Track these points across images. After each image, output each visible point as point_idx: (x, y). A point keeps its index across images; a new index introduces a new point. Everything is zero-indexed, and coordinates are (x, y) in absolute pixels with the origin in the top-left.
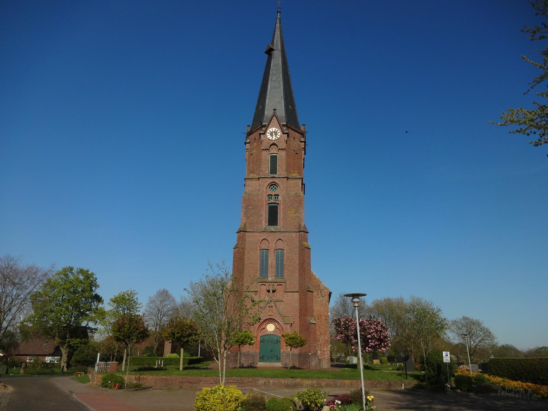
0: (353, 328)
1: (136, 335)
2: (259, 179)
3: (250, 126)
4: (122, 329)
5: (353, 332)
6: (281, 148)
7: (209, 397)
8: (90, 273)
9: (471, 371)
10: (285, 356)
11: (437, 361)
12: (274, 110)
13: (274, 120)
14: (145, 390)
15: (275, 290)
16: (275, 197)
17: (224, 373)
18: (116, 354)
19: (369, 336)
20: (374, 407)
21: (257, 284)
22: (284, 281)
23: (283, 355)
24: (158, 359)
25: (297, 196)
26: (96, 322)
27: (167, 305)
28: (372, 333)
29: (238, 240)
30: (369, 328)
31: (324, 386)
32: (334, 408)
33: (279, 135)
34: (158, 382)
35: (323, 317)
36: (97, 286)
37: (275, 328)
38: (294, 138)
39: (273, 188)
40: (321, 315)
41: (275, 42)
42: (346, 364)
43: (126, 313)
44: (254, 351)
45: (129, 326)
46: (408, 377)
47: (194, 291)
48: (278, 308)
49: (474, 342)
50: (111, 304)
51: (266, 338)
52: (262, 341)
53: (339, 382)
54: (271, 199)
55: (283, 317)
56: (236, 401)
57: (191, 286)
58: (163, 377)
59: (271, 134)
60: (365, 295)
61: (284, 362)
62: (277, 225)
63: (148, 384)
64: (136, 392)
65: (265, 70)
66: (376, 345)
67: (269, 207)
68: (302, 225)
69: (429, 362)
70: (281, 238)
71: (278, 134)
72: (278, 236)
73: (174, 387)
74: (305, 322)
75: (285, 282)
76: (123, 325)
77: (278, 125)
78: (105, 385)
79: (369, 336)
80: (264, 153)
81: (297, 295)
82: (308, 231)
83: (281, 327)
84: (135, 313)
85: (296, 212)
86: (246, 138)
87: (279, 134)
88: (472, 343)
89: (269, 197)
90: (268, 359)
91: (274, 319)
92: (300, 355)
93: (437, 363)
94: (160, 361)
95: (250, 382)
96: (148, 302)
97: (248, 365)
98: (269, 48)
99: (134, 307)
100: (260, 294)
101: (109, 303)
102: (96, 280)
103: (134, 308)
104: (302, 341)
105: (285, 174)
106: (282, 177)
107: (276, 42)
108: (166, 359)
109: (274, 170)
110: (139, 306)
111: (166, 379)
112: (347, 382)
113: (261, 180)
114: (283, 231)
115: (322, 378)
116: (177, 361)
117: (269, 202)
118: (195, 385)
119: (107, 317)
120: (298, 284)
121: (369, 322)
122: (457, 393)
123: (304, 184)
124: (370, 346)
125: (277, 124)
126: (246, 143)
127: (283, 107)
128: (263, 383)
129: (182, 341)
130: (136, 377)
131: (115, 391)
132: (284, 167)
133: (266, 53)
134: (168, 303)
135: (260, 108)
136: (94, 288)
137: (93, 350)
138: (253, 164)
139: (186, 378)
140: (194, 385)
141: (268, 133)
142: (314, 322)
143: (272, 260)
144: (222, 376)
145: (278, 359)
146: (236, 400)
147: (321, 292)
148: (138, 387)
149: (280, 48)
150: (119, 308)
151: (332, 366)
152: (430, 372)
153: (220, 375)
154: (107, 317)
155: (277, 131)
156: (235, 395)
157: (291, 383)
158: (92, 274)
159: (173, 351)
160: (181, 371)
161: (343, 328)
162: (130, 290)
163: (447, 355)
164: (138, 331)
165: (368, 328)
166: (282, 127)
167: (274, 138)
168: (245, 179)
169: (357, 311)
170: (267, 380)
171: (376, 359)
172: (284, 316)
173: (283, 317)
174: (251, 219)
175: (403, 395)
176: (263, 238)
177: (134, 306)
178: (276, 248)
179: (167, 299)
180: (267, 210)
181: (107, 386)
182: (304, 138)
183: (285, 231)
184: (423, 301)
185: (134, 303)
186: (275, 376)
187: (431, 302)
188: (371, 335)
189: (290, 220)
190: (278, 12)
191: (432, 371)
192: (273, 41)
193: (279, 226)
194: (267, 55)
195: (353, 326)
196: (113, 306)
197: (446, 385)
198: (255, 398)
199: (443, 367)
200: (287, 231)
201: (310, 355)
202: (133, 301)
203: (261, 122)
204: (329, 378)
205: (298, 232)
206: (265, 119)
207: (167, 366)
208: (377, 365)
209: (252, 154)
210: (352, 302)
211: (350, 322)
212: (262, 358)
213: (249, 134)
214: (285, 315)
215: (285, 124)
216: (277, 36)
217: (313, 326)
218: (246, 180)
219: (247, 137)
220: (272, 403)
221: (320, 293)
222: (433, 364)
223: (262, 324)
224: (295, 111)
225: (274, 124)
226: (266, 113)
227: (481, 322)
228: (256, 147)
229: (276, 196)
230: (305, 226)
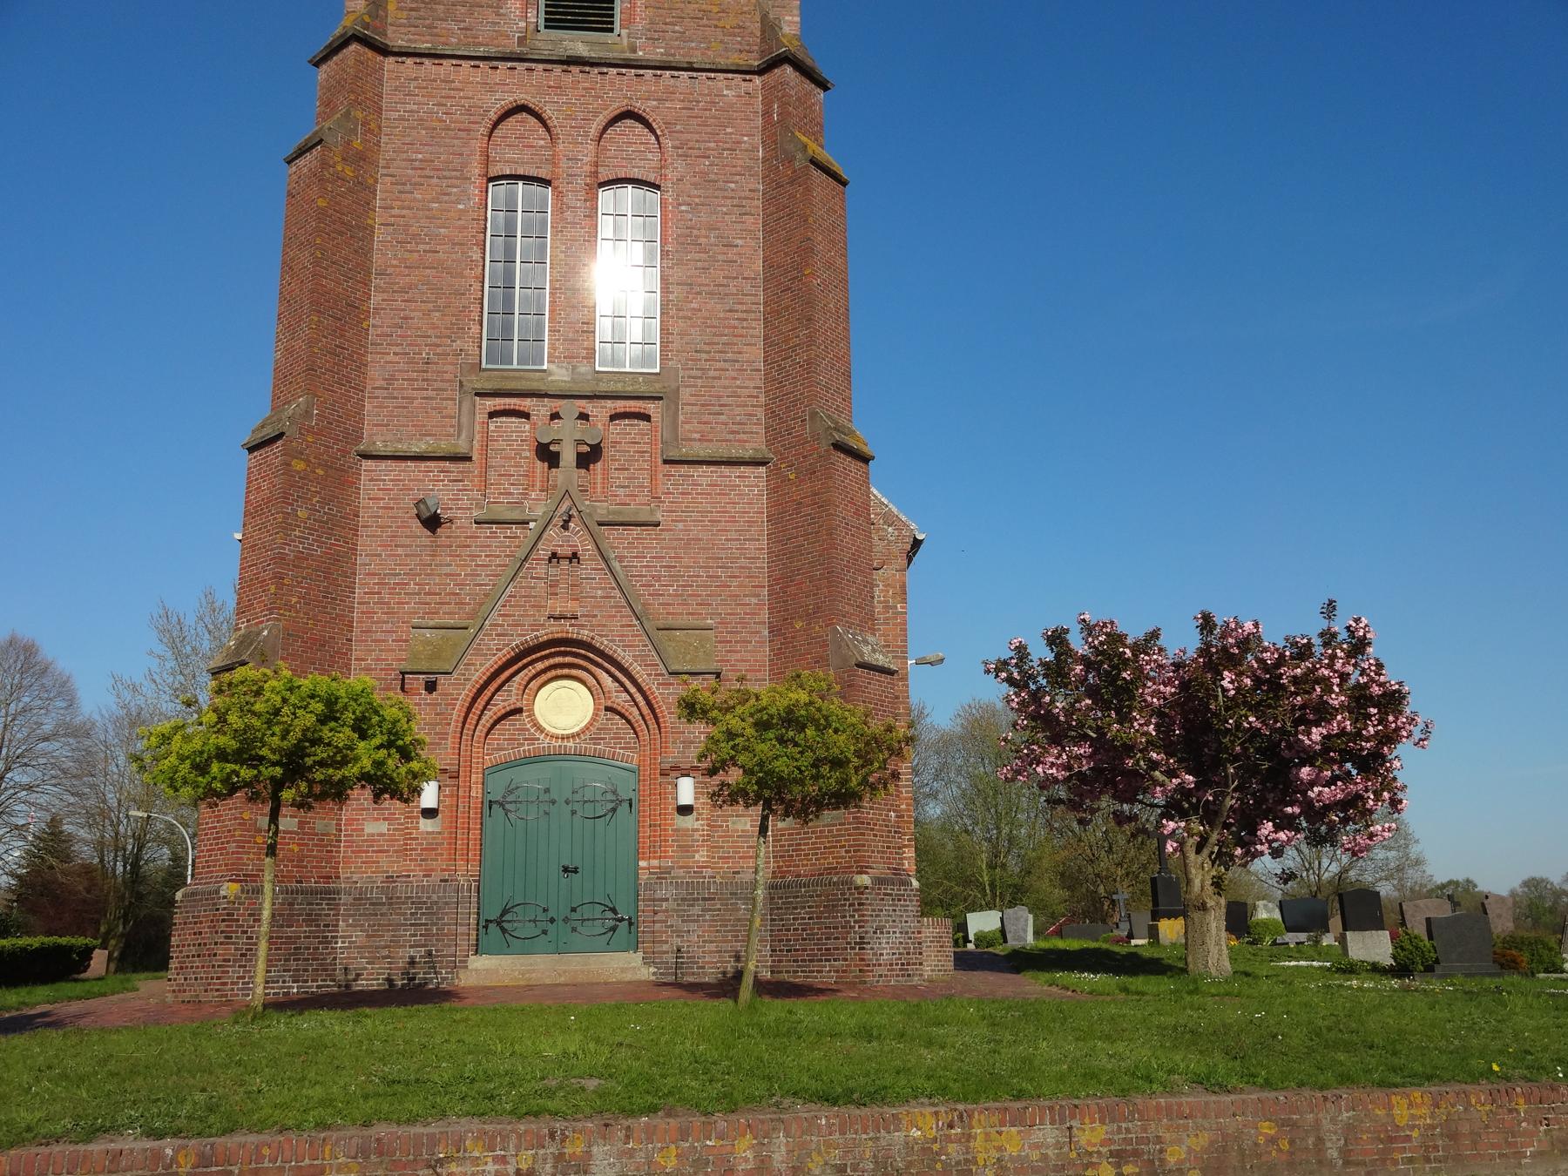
10: (672, 905)
21: (466, 406)
23: (659, 894)
37: (596, 709)
44: (436, 877)
48: (616, 565)
51: (532, 779)
52: (502, 805)
55: (658, 633)
61: (665, 947)
70: (639, 106)
72: (619, 90)
83: (639, 698)
90: (545, 932)
91: (589, 646)
97: (390, 981)
100: (484, 476)
120: (760, 413)
165: (1295, 680)
170: (552, 1149)
172: (661, 624)
173: (658, 633)
176: (508, 100)
193: (624, 32)
201: (861, 890)
205: (760, 72)
212: (499, 923)
214: (671, 622)
223: (499, 681)
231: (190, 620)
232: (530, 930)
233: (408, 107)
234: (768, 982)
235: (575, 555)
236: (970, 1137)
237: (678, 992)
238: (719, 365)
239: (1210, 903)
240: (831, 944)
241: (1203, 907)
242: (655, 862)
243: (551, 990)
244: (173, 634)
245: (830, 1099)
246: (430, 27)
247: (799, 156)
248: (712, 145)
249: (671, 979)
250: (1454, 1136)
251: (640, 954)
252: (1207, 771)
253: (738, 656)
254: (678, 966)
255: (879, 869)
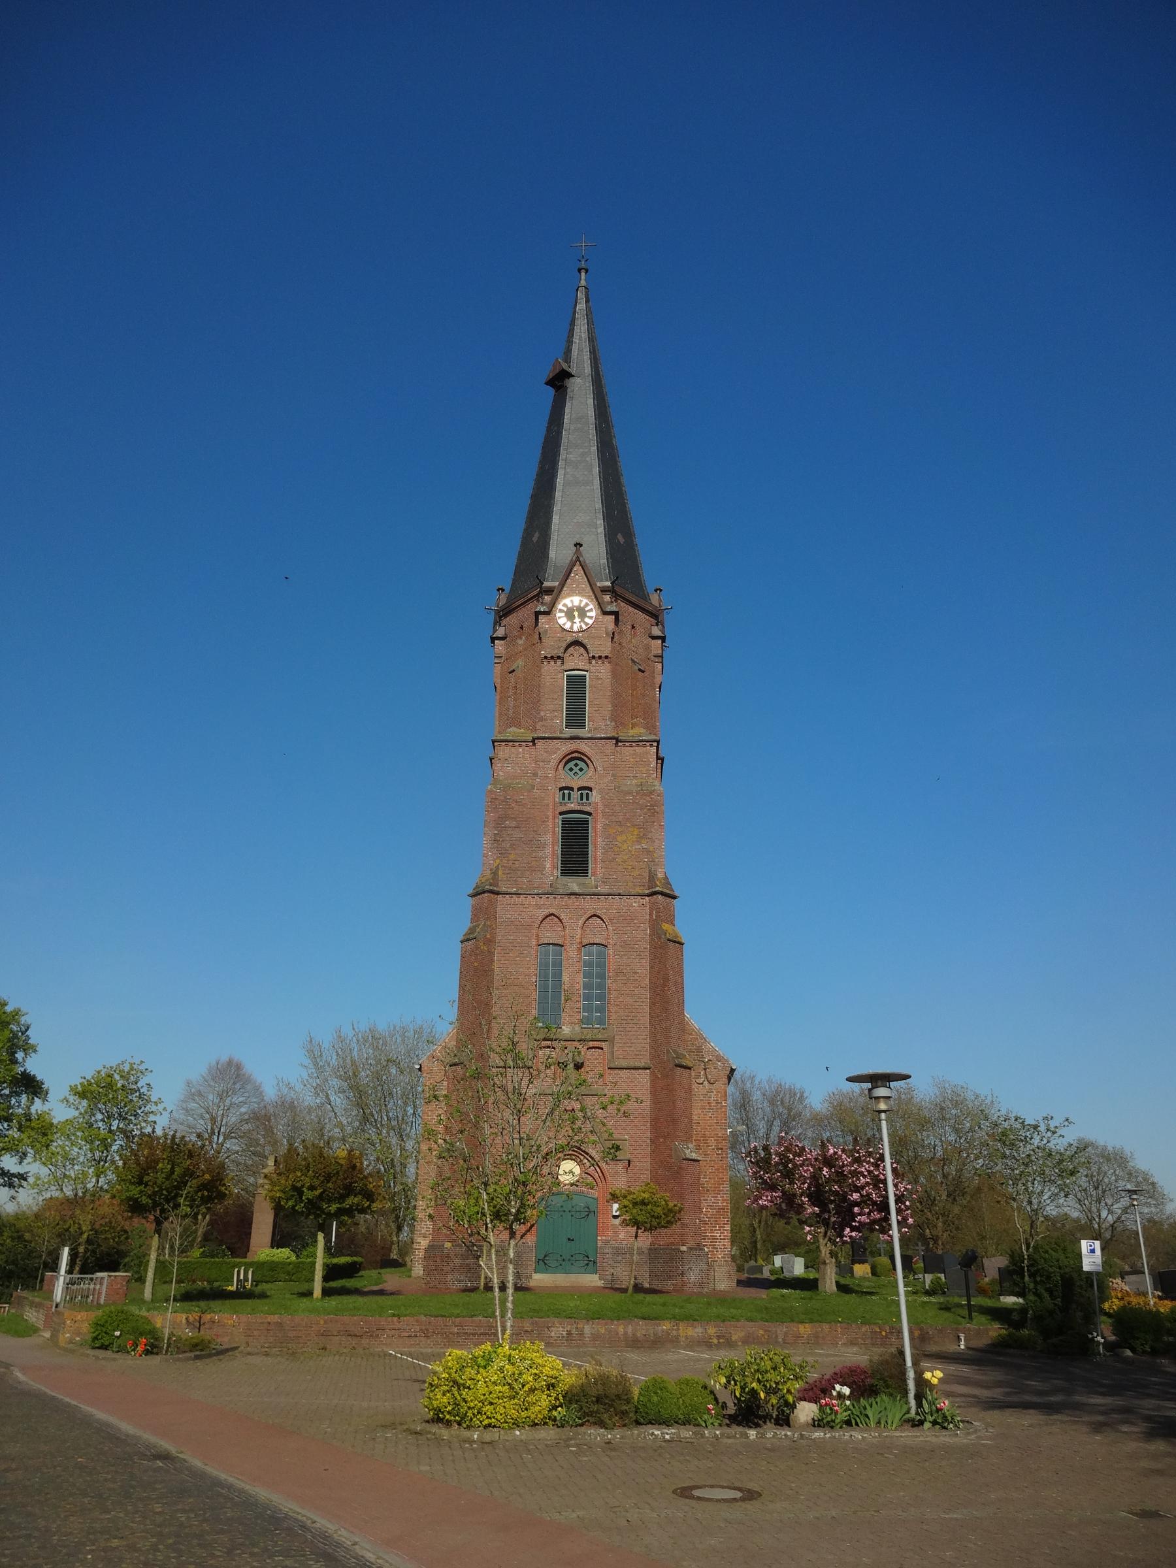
0: (805, 1171)
1: (188, 1193)
2: (533, 741)
3: (503, 590)
4: (148, 1174)
5: (806, 1185)
6: (597, 656)
7: (473, 1379)
8: (8, 1009)
9: (1151, 1297)
11: (1060, 1268)
12: (575, 545)
13: (578, 574)
14: (221, 1357)
15: (583, 1063)
16: (582, 794)
17: (509, 1305)
18: (81, 1249)
19: (856, 1196)
20: (944, 1403)
22: (606, 1035)
24: (238, 1265)
25: (644, 791)
26: (25, 1155)
27: (239, 1106)
28: (863, 1188)
29: (475, 917)
30: (856, 1174)
31: (740, 1343)
32: (831, 1409)
33: (591, 618)
34: (256, 1333)
35: (712, 1142)
36: (28, 1049)
38: (633, 627)
39: (574, 767)
40: (704, 1136)
41: (574, 353)
42: (778, 1279)
43: (114, 1128)
45: (169, 1166)
46: (974, 1314)
47: (316, 1064)
49: (1110, 1212)
50: (72, 1101)
53: (781, 1330)
54: (569, 799)
56: (548, 1389)
57: (310, 1051)
58: (271, 1319)
59: (569, 613)
60: (907, 1077)
61: (607, 1273)
62: (586, 874)
63: (226, 1339)
64: (199, 1363)
65: (547, 431)
66: (874, 1222)
67: (565, 823)
68: (659, 876)
69: (1038, 1270)
70: (599, 912)
71: (588, 614)
72: (591, 905)
73: (303, 1347)
74: (670, 1156)
75: (610, 1040)
76: (151, 1164)
77: (589, 588)
78: (101, 1341)
79: (856, 1196)
80: (549, 668)
81: (644, 1077)
82: (676, 893)
83: (598, 1169)
84: (141, 1128)
85: (641, 838)
86: (495, 624)
87: (593, 614)
88: (1104, 1214)
89: (564, 794)
92: (653, 1253)
93: (1062, 1272)
94: (253, 1272)
95: (527, 1331)
96: (182, 1098)
98: (557, 371)
99: (139, 1111)
101: (65, 1098)
102: (26, 1030)
103: (138, 1114)
104: (670, 1211)
105: (610, 728)
106: (601, 738)
107: (575, 357)
108: (259, 1266)
109: (576, 717)
110: (154, 1108)
111: (280, 1325)
112: (805, 1330)
113: (539, 744)
114: (606, 891)
115: (733, 1318)
116: (302, 1272)
117: (564, 809)
118: (365, 1342)
119: (59, 1141)
120: (647, 1046)
121: (853, 1156)
122: (1126, 1361)
123: (663, 759)
124: (857, 1224)
125: (585, 585)
126: (493, 640)
127: (602, 539)
128: (564, 1333)
129: (323, 1211)
130: (191, 1319)
131: (138, 1362)
132: (608, 709)
133: (550, 383)
134: (241, 1099)
135: (535, 539)
136: (20, 1055)
137: (13, 1239)
138: (515, 700)
139: (337, 1321)
140: (363, 1342)
141: (561, 611)
142: (694, 1156)
143: (572, 974)
144: (503, 1316)
145: (590, 1264)
146: (551, 1386)
147: (705, 1069)
148: (200, 1350)
149: (588, 369)
150: (94, 1115)
151: (740, 1283)
152: (1042, 1301)
153: (498, 1314)
154: (59, 1141)
155: (587, 605)
156: (547, 1371)
157: (645, 1335)
158: (17, 1013)
159: (278, 1241)
160: (317, 1299)
161: (779, 1174)
162: (130, 1060)
163: (1093, 1251)
164: (193, 1183)
165: (850, 1172)
166: (599, 593)
167: (578, 625)
168: (494, 742)
169: (884, 1123)
170: (575, 1326)
171: (862, 1262)
174: (512, 857)
175: (977, 1368)
176: (547, 912)
177: (140, 1108)
178: (585, 942)
179: (238, 1086)
180: (559, 830)
181: (107, 1346)
182: (660, 626)
183: (611, 891)
184: (970, 1096)
185: (140, 1098)
186: (592, 1317)
187: (992, 1097)
188: (860, 1193)
189: (624, 862)
190: (580, 271)
191: (1046, 1295)
192: (568, 351)
194: (551, 391)
195: (805, 1168)
196: (77, 1109)
197: (1090, 1336)
198: (603, 1379)
199: (1078, 1284)
200: (617, 892)
201: (683, 1252)
202: (138, 1094)
203: (540, 580)
204: (750, 1320)
205: (648, 896)
206: (550, 570)
207: (263, 1287)
208: (863, 1278)
209: (514, 671)
210: (871, 1098)
211: (800, 1156)
213: (503, 613)
215: (608, 587)
216: (581, 337)
217: (691, 1167)
218: (496, 744)
219: (497, 623)
220: (655, 1393)
221: (702, 1073)
222: (1049, 1277)
224: (634, 549)
225: (577, 586)
226: (552, 554)
227: (1129, 1154)
228: (525, 649)
229: (585, 792)
230: (666, 878)
231: (326, 1045)
232: (555, 1264)
233: (507, 916)
234: (647, 1289)
235: (573, 1110)
236: (679, 1329)
237: (612, 1291)
238: (630, 1026)
239: (827, 1261)
240: (671, 1274)
241: (825, 1263)
242: (604, 1238)
243: (564, 1288)
244: (314, 1052)
245: (644, 1318)
246: (516, 881)
247: (663, 936)
248: (629, 928)
249: (610, 1286)
250: (817, 1337)
251: (598, 1275)
252: (824, 1208)
253: (637, 1152)
254: (612, 1281)
255: (691, 1244)
